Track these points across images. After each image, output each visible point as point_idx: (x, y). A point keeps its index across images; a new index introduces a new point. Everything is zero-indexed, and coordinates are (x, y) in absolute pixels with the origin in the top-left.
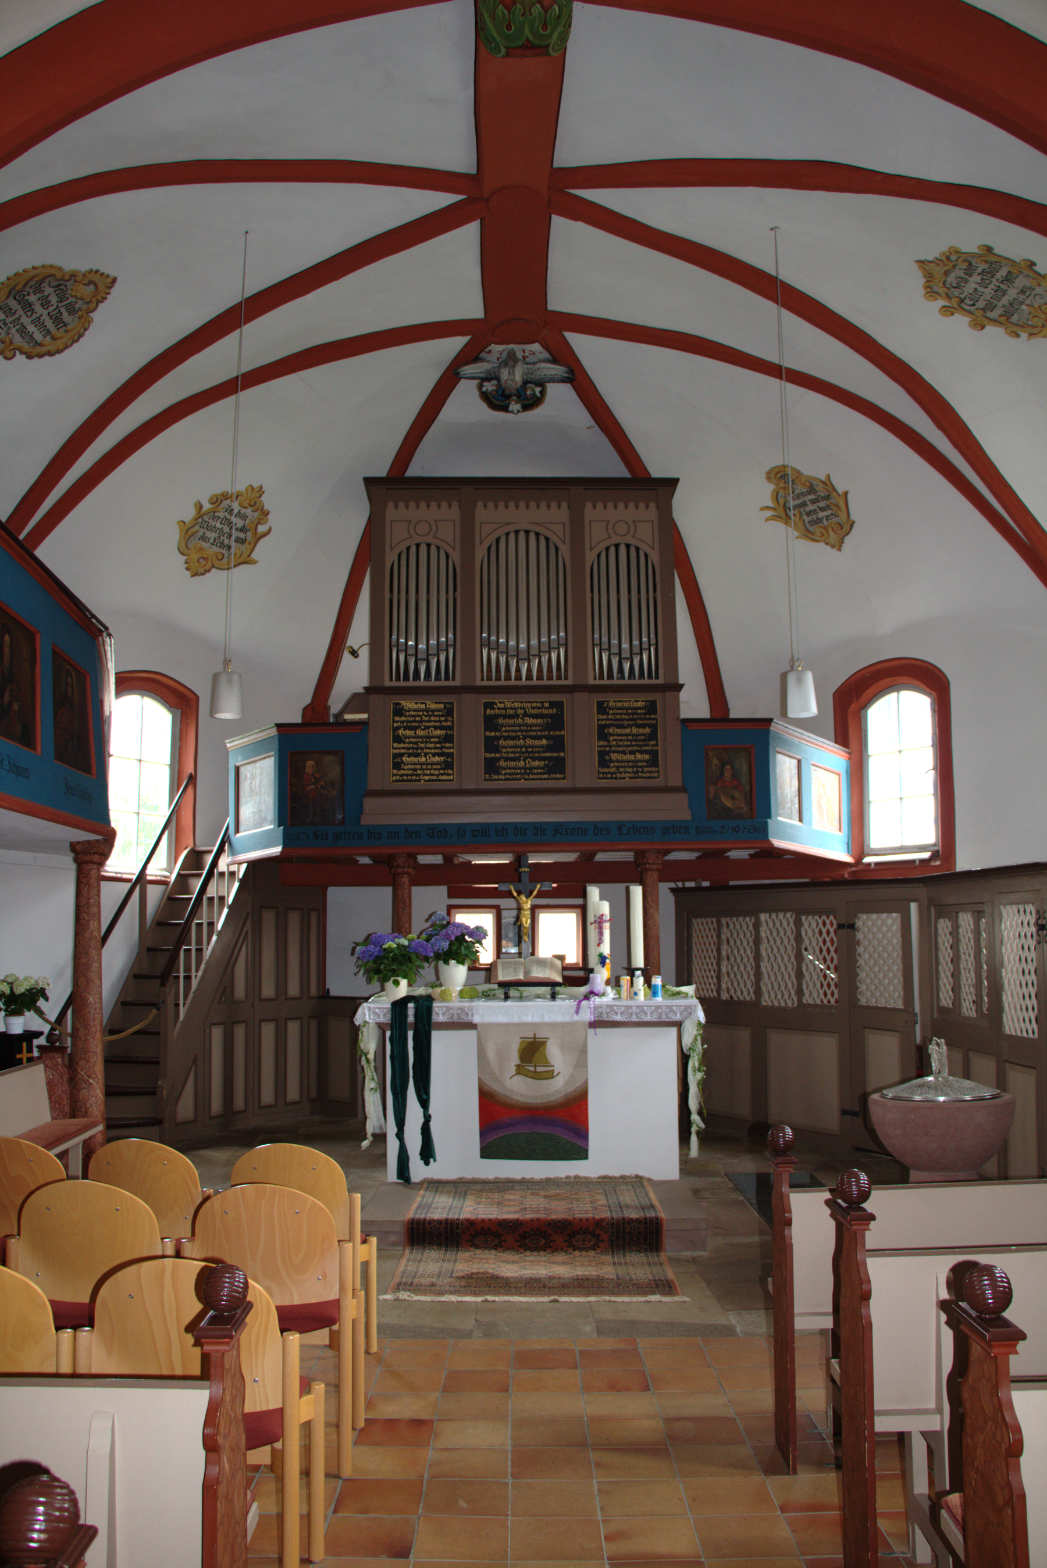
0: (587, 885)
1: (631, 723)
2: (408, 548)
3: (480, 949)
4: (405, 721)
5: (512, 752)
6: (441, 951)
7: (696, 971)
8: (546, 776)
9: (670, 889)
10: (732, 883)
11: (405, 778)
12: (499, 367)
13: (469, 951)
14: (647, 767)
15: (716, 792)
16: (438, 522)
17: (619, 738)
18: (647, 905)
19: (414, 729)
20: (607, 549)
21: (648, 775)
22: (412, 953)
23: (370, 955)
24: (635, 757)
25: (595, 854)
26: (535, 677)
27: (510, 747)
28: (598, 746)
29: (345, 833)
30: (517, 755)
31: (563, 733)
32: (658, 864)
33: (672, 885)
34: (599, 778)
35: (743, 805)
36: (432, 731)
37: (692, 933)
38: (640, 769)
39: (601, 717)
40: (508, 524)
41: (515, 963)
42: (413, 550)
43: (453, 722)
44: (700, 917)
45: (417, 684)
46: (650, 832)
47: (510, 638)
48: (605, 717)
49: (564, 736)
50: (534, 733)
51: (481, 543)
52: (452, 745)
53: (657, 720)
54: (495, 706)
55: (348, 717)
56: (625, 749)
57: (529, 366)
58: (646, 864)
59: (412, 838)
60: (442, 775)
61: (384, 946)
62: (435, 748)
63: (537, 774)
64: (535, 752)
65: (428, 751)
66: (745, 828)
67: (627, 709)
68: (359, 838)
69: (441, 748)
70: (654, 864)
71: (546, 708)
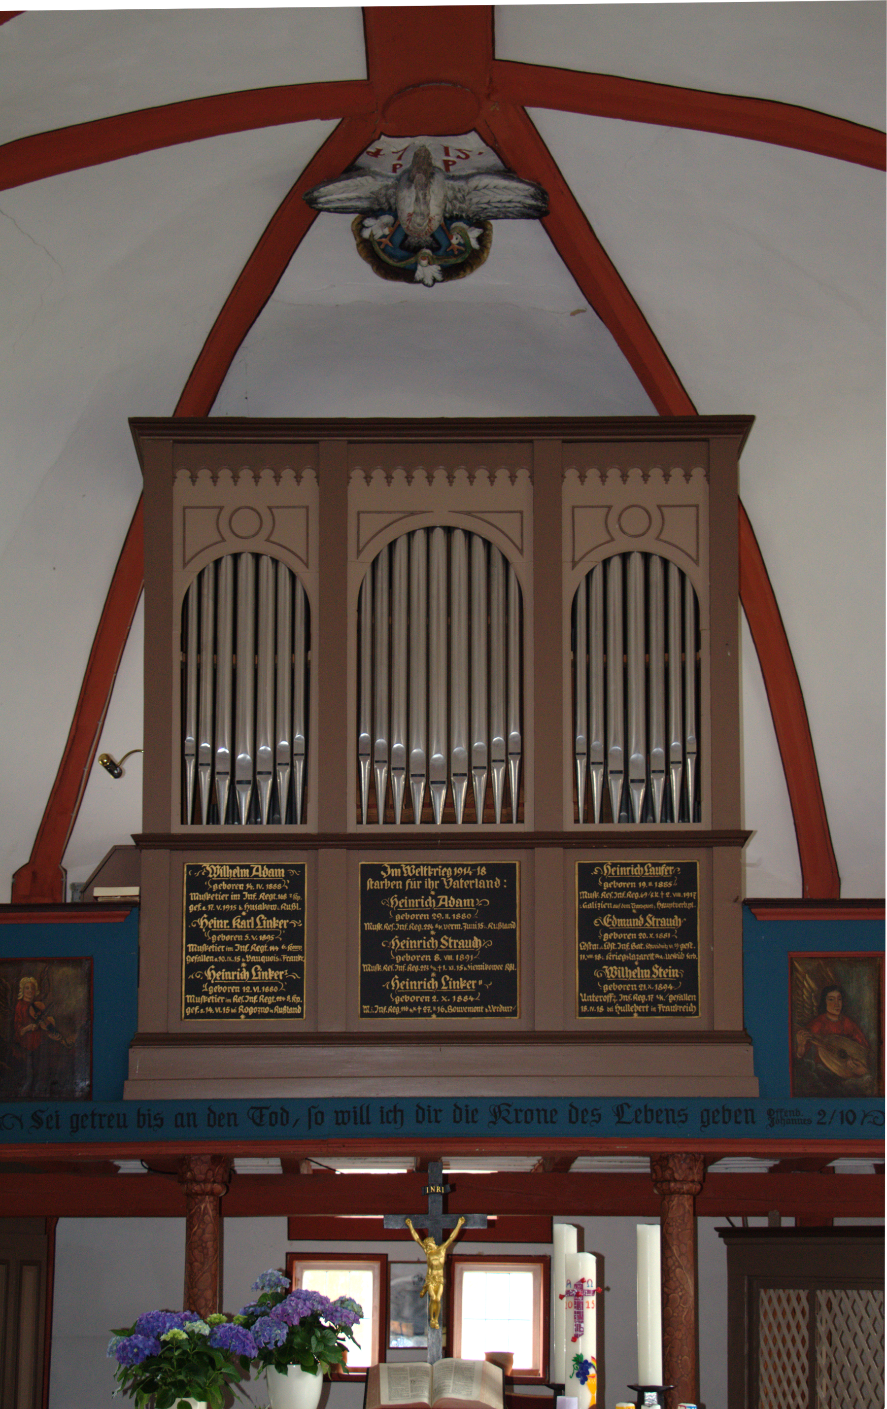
0: (555, 1218)
1: (646, 906)
2: (217, 563)
3: (348, 1343)
4: (210, 902)
5: (415, 963)
6: (271, 1347)
7: (766, 1395)
8: (478, 1009)
9: (717, 1229)
10: (839, 1222)
11: (210, 1010)
12: (397, 186)
13: (326, 1346)
14: (673, 992)
15: (808, 1044)
16: (273, 510)
17: (620, 936)
18: (670, 1262)
19: (228, 916)
20: (606, 563)
21: (675, 1008)
22: (217, 1349)
23: (137, 1355)
24: (652, 973)
25: (572, 1160)
26: (460, 819)
27: (411, 953)
28: (581, 952)
29: (93, 1114)
30: (424, 968)
31: (512, 925)
32: (693, 1181)
33: (722, 1222)
34: (582, 1014)
35: (862, 1070)
36: (261, 920)
37: (758, 1318)
38: (661, 998)
39: (586, 894)
40: (412, 514)
41: (414, 1372)
42: (227, 567)
43: (301, 903)
44: (775, 1287)
45: (233, 829)
46: (677, 1119)
47: (414, 742)
48: (595, 895)
49: (514, 931)
50: (457, 926)
51: (359, 552)
52: (300, 947)
53: (695, 902)
54: (382, 873)
55: (100, 892)
56: (632, 957)
57: (457, 184)
58: (669, 1181)
59: (220, 1125)
60: (281, 1004)
61: (163, 1337)
62: (268, 953)
63: (462, 1004)
64: (459, 963)
65: (254, 959)
66: (865, 1116)
67: (637, 880)
68: (119, 1126)
69: (279, 953)
70: (683, 1181)
71: (480, 878)
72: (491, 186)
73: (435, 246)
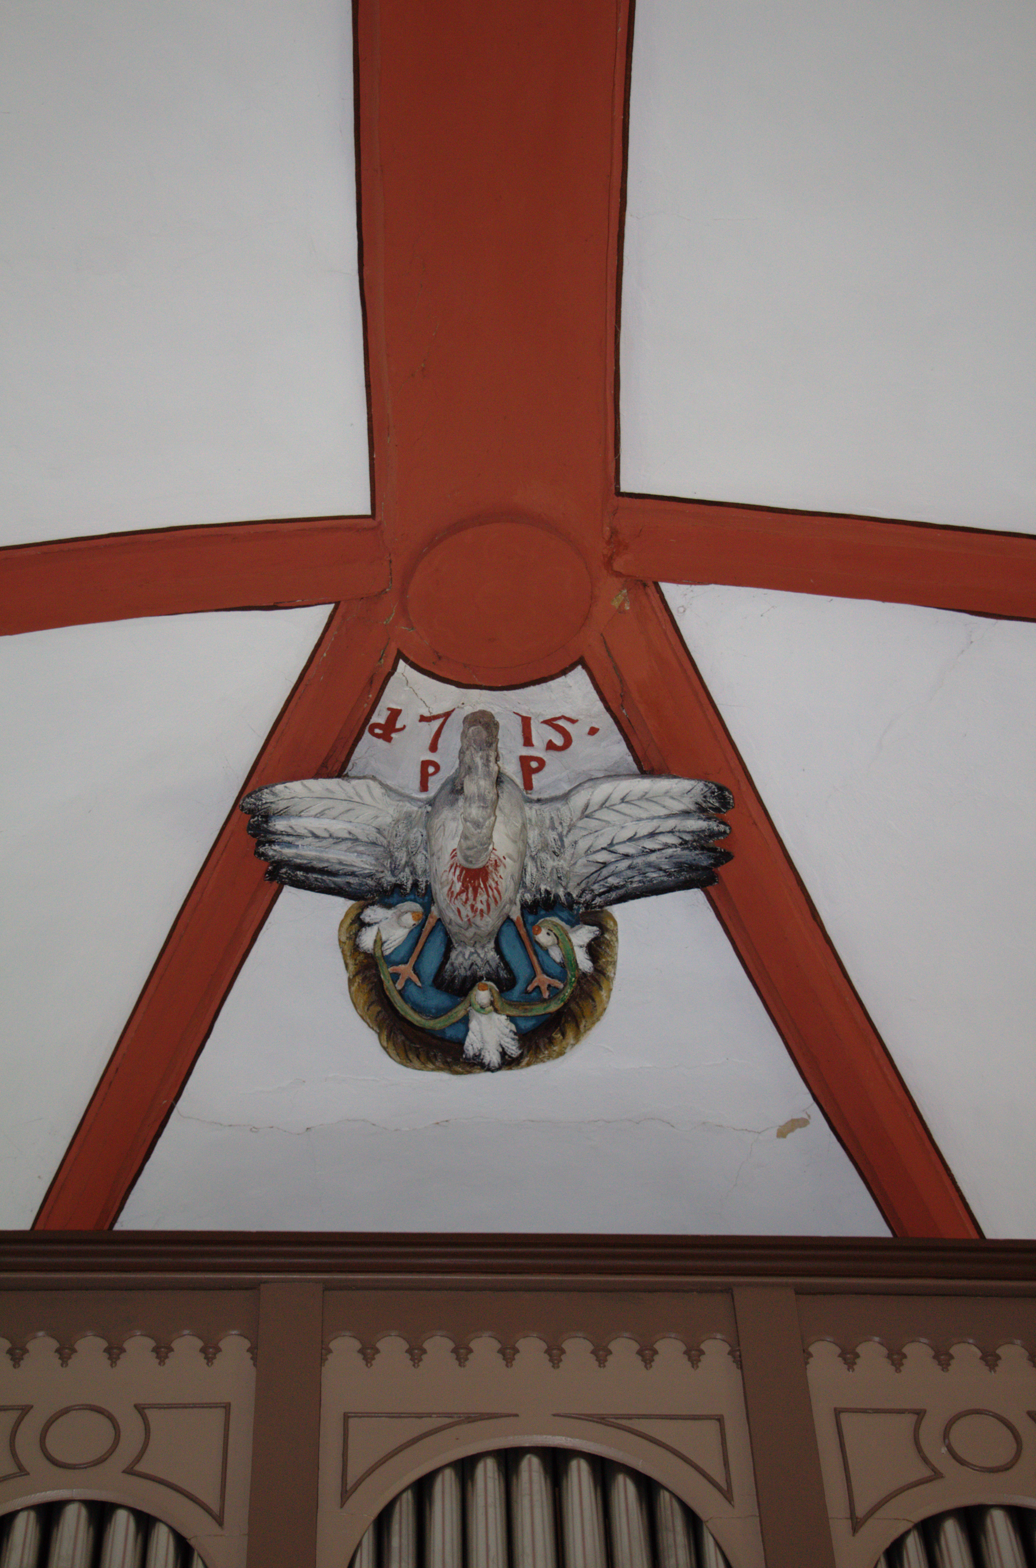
40: (471, 1418)
51: (345, 1494)
72: (616, 797)
73: (503, 974)
